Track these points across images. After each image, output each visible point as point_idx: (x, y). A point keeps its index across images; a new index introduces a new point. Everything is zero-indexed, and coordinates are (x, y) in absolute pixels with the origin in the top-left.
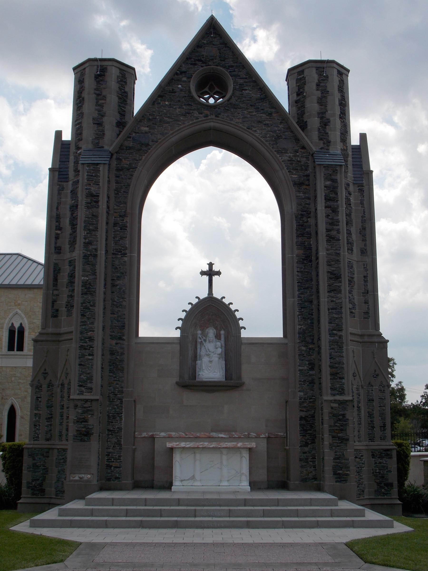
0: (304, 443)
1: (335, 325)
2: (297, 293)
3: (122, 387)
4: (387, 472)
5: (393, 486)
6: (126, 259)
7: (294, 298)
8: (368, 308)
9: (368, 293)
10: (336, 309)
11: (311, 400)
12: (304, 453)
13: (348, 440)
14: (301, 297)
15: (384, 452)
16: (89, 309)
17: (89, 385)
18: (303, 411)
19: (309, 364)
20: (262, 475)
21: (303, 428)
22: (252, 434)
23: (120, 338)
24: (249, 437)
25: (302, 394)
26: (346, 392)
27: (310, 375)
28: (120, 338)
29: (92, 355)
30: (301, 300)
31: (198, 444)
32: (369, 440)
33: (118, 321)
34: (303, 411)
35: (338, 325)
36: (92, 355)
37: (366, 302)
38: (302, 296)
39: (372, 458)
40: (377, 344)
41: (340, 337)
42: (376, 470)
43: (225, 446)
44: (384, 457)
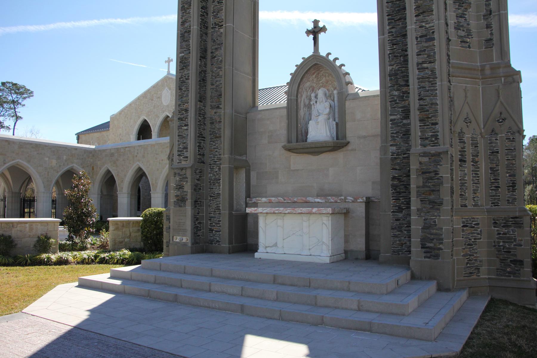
0: (397, 208)
1: (426, 56)
2: (388, 28)
3: (220, 155)
4: (515, 245)
5: (523, 264)
6: (222, 30)
7: (383, 35)
8: (492, 34)
9: (490, 14)
10: (427, 37)
11: (405, 156)
12: (396, 220)
13: (441, 204)
14: (392, 32)
15: (511, 220)
16: (185, 82)
17: (186, 154)
18: (396, 169)
19: (403, 112)
20: (359, 244)
21: (395, 189)
22: (349, 198)
23: (218, 107)
24: (346, 202)
25: (394, 148)
26: (441, 141)
27: (404, 124)
28: (218, 107)
29: (187, 125)
30: (392, 35)
31: (274, 209)
32: (492, 203)
33: (216, 91)
34: (396, 169)
35: (429, 56)
36: (187, 125)
37: (488, 26)
38: (393, 30)
39: (494, 227)
40: (503, 79)
41: (433, 71)
42: (499, 242)
43: (300, 212)
44: (510, 226)
